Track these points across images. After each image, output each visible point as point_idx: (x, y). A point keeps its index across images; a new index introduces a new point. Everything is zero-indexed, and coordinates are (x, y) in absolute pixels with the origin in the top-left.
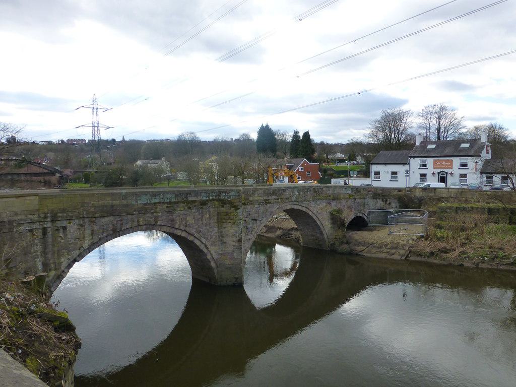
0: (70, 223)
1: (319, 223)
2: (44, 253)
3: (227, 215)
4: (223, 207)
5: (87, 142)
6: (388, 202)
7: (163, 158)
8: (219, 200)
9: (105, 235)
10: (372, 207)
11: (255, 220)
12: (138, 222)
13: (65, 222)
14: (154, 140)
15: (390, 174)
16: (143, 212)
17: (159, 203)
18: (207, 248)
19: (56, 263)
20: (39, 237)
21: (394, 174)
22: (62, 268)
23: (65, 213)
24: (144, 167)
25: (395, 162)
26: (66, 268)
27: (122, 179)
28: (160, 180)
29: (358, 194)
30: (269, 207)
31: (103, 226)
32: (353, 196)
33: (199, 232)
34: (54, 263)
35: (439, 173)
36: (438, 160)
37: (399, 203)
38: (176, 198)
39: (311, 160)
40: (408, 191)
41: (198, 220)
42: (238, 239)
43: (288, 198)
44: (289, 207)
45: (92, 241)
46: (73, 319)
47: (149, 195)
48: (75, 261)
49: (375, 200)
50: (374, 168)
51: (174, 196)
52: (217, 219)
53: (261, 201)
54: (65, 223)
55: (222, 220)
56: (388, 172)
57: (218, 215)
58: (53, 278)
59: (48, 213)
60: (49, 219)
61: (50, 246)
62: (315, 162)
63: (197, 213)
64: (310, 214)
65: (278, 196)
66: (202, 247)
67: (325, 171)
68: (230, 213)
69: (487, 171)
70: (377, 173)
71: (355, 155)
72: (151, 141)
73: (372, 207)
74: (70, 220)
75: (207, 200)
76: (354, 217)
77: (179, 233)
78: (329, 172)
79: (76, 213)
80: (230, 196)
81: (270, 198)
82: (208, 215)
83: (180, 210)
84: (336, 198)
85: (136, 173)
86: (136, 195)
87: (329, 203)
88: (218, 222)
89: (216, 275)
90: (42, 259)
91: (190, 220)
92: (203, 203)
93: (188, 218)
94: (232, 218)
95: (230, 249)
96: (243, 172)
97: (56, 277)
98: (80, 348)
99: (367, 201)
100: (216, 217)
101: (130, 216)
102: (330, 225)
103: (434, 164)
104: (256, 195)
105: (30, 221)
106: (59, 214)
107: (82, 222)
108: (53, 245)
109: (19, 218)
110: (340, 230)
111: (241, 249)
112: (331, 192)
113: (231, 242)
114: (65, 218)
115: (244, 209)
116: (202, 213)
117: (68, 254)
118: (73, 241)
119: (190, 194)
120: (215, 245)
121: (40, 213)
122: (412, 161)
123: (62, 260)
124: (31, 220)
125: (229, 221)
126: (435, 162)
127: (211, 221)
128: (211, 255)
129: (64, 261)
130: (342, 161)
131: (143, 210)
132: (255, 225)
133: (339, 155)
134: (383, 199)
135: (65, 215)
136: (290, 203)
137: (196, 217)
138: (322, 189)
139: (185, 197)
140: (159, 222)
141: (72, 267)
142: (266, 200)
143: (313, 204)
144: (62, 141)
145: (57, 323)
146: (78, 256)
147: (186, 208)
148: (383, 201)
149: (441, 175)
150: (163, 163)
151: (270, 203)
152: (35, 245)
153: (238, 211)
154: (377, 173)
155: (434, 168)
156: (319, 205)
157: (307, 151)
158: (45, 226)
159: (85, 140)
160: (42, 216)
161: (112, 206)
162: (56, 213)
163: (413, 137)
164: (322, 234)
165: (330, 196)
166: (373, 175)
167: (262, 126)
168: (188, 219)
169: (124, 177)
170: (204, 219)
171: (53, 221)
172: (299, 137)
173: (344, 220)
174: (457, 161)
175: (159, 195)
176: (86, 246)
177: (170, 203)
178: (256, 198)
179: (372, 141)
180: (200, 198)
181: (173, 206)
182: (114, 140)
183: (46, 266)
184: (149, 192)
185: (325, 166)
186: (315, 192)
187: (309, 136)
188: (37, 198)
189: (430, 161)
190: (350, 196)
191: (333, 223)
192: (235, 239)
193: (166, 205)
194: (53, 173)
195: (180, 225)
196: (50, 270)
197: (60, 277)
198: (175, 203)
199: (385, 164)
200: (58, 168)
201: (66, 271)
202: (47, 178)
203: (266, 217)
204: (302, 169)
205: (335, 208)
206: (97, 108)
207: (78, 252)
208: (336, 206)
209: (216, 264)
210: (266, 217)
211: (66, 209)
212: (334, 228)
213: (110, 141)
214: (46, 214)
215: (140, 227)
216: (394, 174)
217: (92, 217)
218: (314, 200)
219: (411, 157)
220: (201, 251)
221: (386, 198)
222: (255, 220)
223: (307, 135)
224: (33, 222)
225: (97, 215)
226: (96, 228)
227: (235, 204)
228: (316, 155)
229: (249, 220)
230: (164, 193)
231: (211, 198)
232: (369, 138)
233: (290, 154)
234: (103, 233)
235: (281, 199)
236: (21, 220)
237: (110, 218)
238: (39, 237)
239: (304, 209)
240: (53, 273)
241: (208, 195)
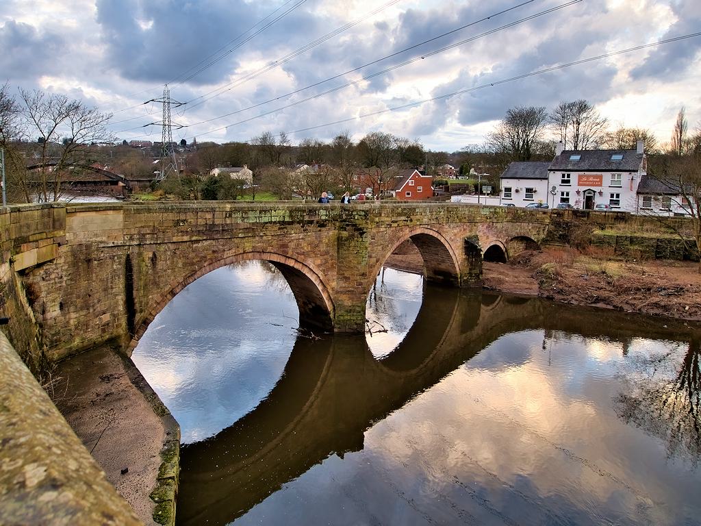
1: (451, 253)
25: (524, 176)
35: (584, 192)
50: (505, 184)
69: (644, 191)
77: (291, 263)
122: (551, 175)
149: (587, 194)
154: (508, 190)
174: (607, 176)
181: (286, 228)
189: (574, 177)
236: (101, 242)
239: (436, 235)
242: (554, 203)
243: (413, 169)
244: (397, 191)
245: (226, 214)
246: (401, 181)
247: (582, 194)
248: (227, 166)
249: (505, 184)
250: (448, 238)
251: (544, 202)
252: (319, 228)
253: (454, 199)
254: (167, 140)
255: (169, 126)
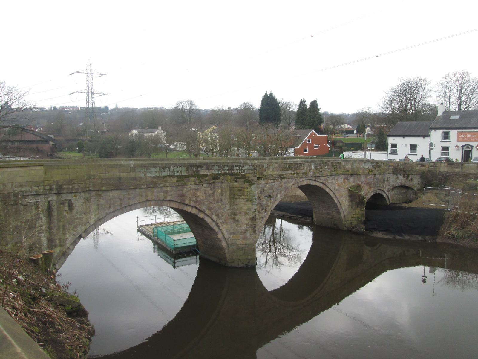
0: (75, 196)
1: (336, 201)
2: (50, 228)
3: (240, 190)
4: (236, 181)
5: (79, 109)
6: (410, 178)
7: (160, 128)
8: (232, 174)
9: (111, 210)
10: (392, 184)
11: (270, 196)
12: (147, 196)
13: (70, 195)
14: (148, 108)
15: (408, 148)
16: (151, 186)
17: (169, 176)
18: (218, 227)
19: (61, 238)
20: (44, 211)
21: (413, 147)
22: (68, 245)
23: (71, 185)
24: (140, 136)
25: (415, 134)
26: (71, 244)
27: (117, 149)
28: (157, 150)
29: (377, 169)
30: (285, 183)
31: (110, 200)
32: (372, 171)
33: (210, 209)
34: (60, 239)
35: (463, 147)
36: (463, 133)
37: (421, 179)
38: (187, 172)
39: (320, 131)
40: (432, 166)
41: (210, 195)
42: (251, 217)
43: (305, 173)
44: (305, 183)
45: (98, 216)
46: (86, 306)
47: (158, 168)
48: (81, 237)
49: (395, 176)
50: (391, 141)
51: (184, 169)
52: (230, 195)
53: (276, 176)
54: (70, 197)
55: (234, 195)
56: (406, 145)
57: (230, 190)
58: (58, 255)
59: (53, 185)
60: (54, 192)
61: (55, 220)
62: (323, 134)
63: (208, 189)
64: (327, 190)
65: (293, 171)
66: (213, 225)
67: (333, 143)
68: (244, 188)
70: (394, 146)
71: (364, 126)
72: (144, 109)
73: (392, 184)
74: (76, 193)
75: (219, 174)
76: (372, 194)
77: (189, 209)
78: (338, 144)
79: (82, 186)
80: (244, 170)
81: (285, 172)
82: (220, 191)
83: (191, 184)
84: (354, 174)
85: (132, 142)
86: (146, 167)
87: (348, 179)
88: (230, 198)
89: (227, 255)
90: (47, 234)
91: (201, 195)
92: (216, 177)
93: (199, 193)
94: (245, 194)
95: (244, 228)
96: (249, 143)
97: (61, 254)
98: (93, 335)
99: (387, 176)
100: (228, 193)
101: (138, 190)
102: (347, 203)
103: (458, 137)
104: (271, 169)
105: (35, 193)
106: (65, 187)
107: (88, 196)
108: (59, 221)
109: (24, 189)
110: (359, 209)
111: (255, 227)
112: (349, 166)
113: (243, 219)
114: (71, 192)
115: (258, 184)
116: (214, 188)
117: (73, 230)
118: (79, 216)
119: (201, 167)
120: (227, 223)
121: (45, 185)
122: (433, 133)
123: (68, 236)
124: (36, 192)
125: (242, 197)
126: (459, 134)
127: (223, 197)
128: (222, 233)
129: (69, 237)
130: (351, 132)
131: (152, 184)
132: (269, 202)
133: (347, 126)
134: (404, 175)
135: (71, 187)
136: (307, 179)
137: (207, 192)
138: (341, 163)
139: (196, 171)
140: (168, 197)
141: (77, 243)
142: (281, 175)
143: (330, 180)
144: (55, 108)
145: (69, 308)
146: (84, 232)
147: (197, 182)
148: (404, 177)
150: (159, 132)
151: (285, 178)
152: (40, 219)
153: (253, 186)
154: (394, 146)
155: (458, 141)
156: (337, 180)
157: (315, 121)
158: (51, 199)
159: (77, 107)
160: (47, 188)
161: (120, 179)
162: (61, 186)
163: (435, 110)
164: (338, 212)
165: (348, 171)
166: (389, 148)
167: (266, 94)
168: (198, 194)
169: (119, 147)
170: (216, 194)
171: (58, 194)
172: (306, 106)
173: (363, 198)
175: (169, 168)
176: (92, 221)
177: (180, 176)
178: (271, 172)
179: (387, 111)
180: (211, 172)
181: (183, 180)
182: (106, 108)
183: (50, 241)
184: (158, 164)
185: (335, 137)
186: (333, 166)
187: (317, 105)
188: (42, 168)
189: (453, 134)
190: (370, 171)
191: (351, 201)
192: (248, 217)
193: (176, 179)
194: (46, 141)
195: (190, 200)
196: (55, 246)
197: (65, 255)
198: (185, 176)
199: (404, 136)
200: (52, 136)
201: (71, 247)
202: (40, 146)
203: (281, 193)
204: (309, 141)
205: (353, 184)
206: (91, 74)
207: (83, 228)
208: (354, 181)
209: (228, 244)
210: (281, 193)
211: (72, 181)
212: (352, 207)
213: (103, 109)
214: (51, 186)
215: (148, 202)
216: (413, 147)
217: (98, 191)
218: (331, 175)
219: (432, 129)
220: (212, 229)
221: (408, 173)
222: (270, 196)
223: (314, 104)
224: (38, 195)
225: (104, 188)
226: (102, 202)
227: (249, 179)
228: (322, 126)
229: (263, 196)
230: (174, 165)
231: (223, 172)
232: (383, 108)
233: (296, 124)
234: (110, 207)
235: (298, 174)
236: (26, 191)
237: (117, 192)
238: (44, 211)
239: (321, 185)
240: (57, 250)
241: (220, 168)
242: (436, 155)
243: (310, 129)
244: (295, 148)
245: (130, 169)
246: (299, 139)
247: (461, 148)
248: (142, 128)
249: (391, 141)
250: (332, 188)
251: (426, 156)
252: (213, 181)
253: (346, 154)
254: (91, 106)
255: (92, 93)
